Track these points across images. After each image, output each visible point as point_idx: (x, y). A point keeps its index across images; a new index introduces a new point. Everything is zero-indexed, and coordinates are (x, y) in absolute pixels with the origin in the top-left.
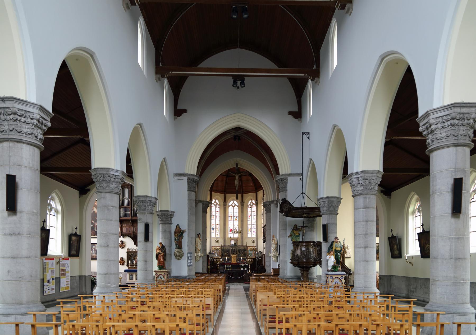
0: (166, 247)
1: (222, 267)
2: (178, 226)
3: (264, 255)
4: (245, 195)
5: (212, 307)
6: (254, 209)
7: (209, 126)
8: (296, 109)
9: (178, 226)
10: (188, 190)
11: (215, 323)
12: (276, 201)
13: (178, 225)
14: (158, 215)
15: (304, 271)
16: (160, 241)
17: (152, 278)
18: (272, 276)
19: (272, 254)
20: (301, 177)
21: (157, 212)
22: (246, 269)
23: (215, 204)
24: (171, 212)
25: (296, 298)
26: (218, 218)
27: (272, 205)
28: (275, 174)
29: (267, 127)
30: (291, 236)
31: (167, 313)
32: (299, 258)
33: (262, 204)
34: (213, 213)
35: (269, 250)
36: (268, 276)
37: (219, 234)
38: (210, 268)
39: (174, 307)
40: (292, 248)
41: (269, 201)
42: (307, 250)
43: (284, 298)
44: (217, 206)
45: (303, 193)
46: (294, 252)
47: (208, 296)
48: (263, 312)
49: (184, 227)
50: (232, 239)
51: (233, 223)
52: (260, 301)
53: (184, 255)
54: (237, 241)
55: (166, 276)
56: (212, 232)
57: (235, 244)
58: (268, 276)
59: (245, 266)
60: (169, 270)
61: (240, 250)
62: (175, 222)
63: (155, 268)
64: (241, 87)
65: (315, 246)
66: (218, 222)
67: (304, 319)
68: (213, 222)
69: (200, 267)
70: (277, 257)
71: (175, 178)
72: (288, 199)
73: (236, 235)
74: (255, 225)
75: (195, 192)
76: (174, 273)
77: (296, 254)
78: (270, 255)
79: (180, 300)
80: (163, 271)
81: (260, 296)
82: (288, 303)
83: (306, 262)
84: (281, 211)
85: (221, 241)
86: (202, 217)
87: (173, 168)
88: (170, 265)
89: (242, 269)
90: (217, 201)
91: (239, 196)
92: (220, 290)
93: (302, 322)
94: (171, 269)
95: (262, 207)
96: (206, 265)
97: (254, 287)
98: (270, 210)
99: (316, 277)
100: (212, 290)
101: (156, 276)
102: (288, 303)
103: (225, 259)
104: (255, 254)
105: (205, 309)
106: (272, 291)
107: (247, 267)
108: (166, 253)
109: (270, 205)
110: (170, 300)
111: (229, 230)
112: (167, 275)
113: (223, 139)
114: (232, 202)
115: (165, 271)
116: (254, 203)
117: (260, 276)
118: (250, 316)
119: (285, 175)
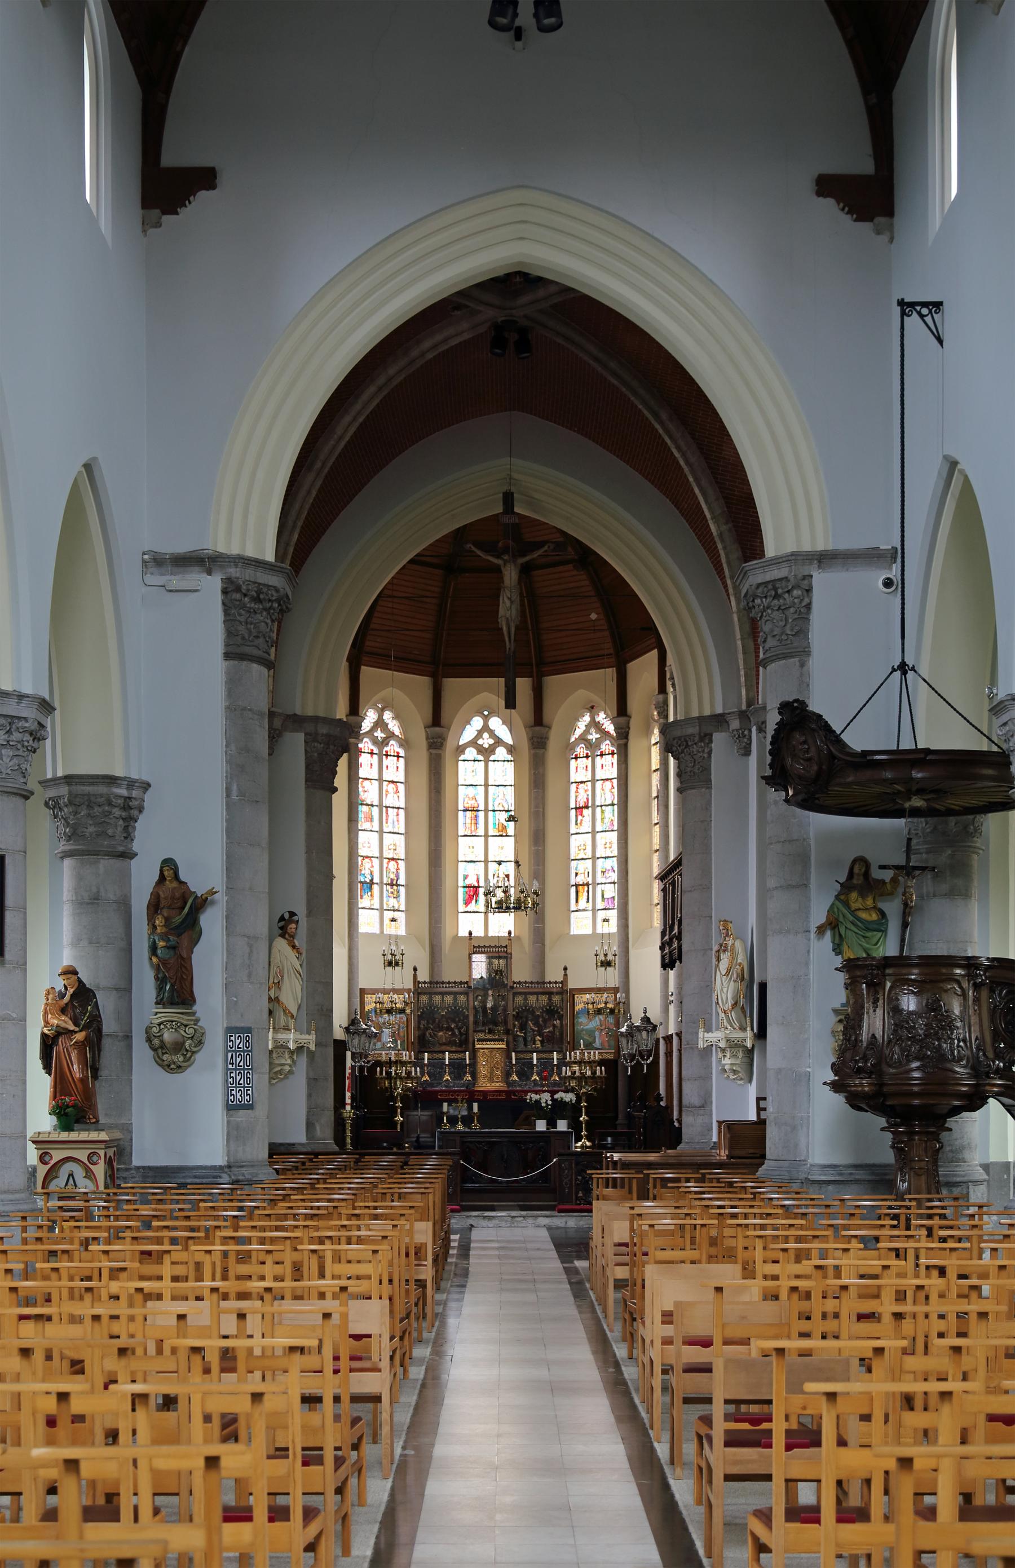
0: (101, 998)
1: (421, 1115)
2: (169, 868)
3: (668, 1039)
4: (553, 682)
5: (382, 1348)
6: (608, 767)
7: (351, 270)
8: (861, 163)
9: (169, 868)
10: (228, 656)
11: (398, 1451)
12: (743, 715)
13: (169, 865)
14: (53, 805)
15: (911, 1134)
16: (67, 959)
17: (20, 1181)
18: (720, 1165)
19: (716, 1036)
20: (894, 573)
21: (45, 783)
22: (562, 1126)
23: (379, 734)
24: (131, 783)
25: (876, 1295)
26: (397, 822)
27: (720, 740)
28: (736, 554)
29: (691, 273)
30: (832, 924)
31: (139, 1388)
32: (881, 1059)
33: (656, 736)
34: (369, 792)
35: (695, 1005)
36: (697, 1166)
37: (401, 916)
38: (357, 1123)
39: (174, 1351)
40: (839, 997)
41: (701, 719)
42: (934, 1009)
43: (808, 1296)
44: (393, 747)
45: (903, 668)
46: (850, 1021)
47: (363, 1287)
48: (687, 1384)
49: (204, 872)
50: (476, 946)
51: (485, 854)
52: (668, 1317)
53: (208, 1040)
54: (507, 957)
55: (99, 1170)
56: (364, 902)
57: (497, 979)
58: (699, 1167)
59: (559, 1109)
60: (117, 1135)
61: (526, 1009)
62: (153, 842)
63: (41, 1119)
64: (543, 29)
65: (977, 987)
66: (396, 844)
67: (946, 1422)
68: (367, 843)
69: (294, 1112)
70: (750, 1052)
71: (150, 579)
72: (815, 706)
73: (503, 924)
74: (614, 863)
75: (270, 665)
76: (146, 1153)
77: (865, 1036)
78: (704, 1038)
79: (200, 1313)
80: (84, 1136)
81: (666, 1288)
82: (831, 1325)
83: (924, 1082)
84: (777, 776)
85: (417, 957)
86: (309, 813)
87: (141, 523)
88: (123, 1105)
89: (541, 1126)
90: (387, 716)
91: (523, 685)
92: (419, 1252)
93: (733, 1441)
94: (127, 1129)
95: (655, 753)
96: (330, 1101)
97: (620, 1231)
98: (706, 770)
99: (980, 1174)
100: (384, 1247)
101: (42, 1170)
102: (831, 1325)
103: (436, 1068)
104: (616, 1037)
105: (344, 1363)
106: (729, 1256)
107: (570, 1111)
108: (99, 1031)
109: (706, 738)
110: (137, 1311)
111: (461, 893)
112: (109, 1162)
113: (427, 344)
114: (477, 722)
115: (94, 1136)
116: (610, 728)
117: (650, 1165)
118: (597, 1409)
119: (794, 558)
